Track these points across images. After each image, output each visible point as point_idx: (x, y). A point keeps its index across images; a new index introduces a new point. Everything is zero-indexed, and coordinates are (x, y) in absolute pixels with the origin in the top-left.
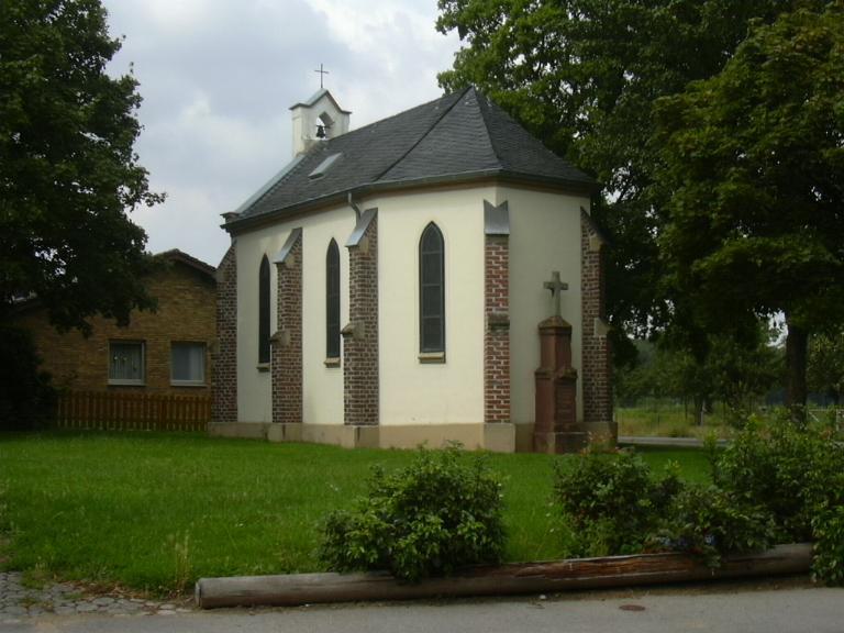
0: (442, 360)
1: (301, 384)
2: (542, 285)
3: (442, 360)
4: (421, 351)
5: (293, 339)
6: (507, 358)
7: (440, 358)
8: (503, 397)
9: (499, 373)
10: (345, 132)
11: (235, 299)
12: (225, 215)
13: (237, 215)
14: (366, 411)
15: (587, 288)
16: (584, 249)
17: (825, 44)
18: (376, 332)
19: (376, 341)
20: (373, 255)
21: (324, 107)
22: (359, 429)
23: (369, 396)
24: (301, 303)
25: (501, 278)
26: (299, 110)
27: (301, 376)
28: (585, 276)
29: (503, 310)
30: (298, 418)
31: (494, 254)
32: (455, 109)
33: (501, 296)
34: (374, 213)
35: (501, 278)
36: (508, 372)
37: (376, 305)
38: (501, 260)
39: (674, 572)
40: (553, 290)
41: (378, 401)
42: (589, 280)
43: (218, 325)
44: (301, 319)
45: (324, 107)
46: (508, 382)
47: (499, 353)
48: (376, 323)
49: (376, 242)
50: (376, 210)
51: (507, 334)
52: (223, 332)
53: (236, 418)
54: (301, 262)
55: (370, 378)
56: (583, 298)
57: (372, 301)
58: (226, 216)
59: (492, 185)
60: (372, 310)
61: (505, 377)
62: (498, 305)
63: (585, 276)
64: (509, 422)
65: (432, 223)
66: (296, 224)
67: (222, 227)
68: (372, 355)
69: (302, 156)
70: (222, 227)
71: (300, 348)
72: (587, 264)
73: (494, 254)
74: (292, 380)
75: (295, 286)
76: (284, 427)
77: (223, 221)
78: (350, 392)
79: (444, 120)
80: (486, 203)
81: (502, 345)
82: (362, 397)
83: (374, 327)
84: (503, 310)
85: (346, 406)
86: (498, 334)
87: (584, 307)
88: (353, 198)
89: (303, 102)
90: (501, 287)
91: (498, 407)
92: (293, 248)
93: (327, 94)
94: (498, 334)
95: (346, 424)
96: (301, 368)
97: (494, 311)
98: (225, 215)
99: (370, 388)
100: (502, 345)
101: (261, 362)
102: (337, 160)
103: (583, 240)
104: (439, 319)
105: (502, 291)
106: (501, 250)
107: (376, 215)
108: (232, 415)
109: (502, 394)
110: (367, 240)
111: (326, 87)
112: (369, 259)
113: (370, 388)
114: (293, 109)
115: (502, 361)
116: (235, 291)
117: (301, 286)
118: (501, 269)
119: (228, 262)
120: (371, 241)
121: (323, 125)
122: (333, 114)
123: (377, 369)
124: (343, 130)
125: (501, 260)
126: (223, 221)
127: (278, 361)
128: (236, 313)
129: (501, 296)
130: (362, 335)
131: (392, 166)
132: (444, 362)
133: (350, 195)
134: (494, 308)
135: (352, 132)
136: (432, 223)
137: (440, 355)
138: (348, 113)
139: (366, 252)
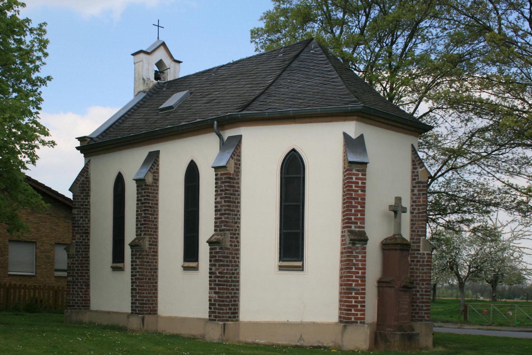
0: (301, 269)
1: (156, 283)
2: (388, 208)
3: (301, 269)
4: (281, 259)
5: (150, 245)
6: (365, 269)
7: (299, 267)
8: (359, 302)
9: (357, 281)
10: (177, 78)
11: (89, 209)
12: (80, 139)
13: (91, 139)
14: (230, 309)
15: (416, 211)
16: (413, 179)
17: (530, 39)
18: (238, 242)
19: (238, 250)
20: (238, 176)
21: (160, 54)
22: (224, 324)
23: (232, 297)
24: (157, 215)
25: (360, 200)
26: (142, 55)
27: (157, 276)
28: (414, 202)
29: (359, 227)
30: (154, 311)
31: (354, 180)
32: (303, 56)
33: (359, 216)
34: (238, 140)
35: (360, 200)
36: (365, 281)
37: (239, 219)
38: (360, 184)
39: (12, 297)
40: (396, 212)
41: (238, 301)
42: (416, 205)
43: (74, 230)
44: (157, 228)
45: (160, 54)
46: (364, 289)
47: (358, 265)
48: (239, 234)
49: (240, 165)
50: (241, 136)
51: (365, 248)
52: (78, 236)
53: (89, 306)
54: (158, 180)
55: (233, 281)
56: (412, 220)
57: (236, 215)
58: (81, 139)
59: (353, 120)
60: (236, 223)
61: (361, 285)
62: (356, 223)
63: (414, 202)
64: (364, 323)
65: (294, 150)
66: (153, 148)
67: (78, 148)
68: (235, 262)
69: (143, 95)
70: (78, 148)
71: (156, 253)
72: (416, 192)
73: (360, 182)
74: (149, 279)
75: (153, 200)
76: (143, 319)
77: (78, 144)
78: (215, 293)
79: (294, 65)
80: (345, 134)
81: (360, 258)
82: (228, 297)
83: (237, 238)
84: (359, 227)
85: (210, 304)
86: (357, 248)
87: (412, 228)
88: (218, 126)
89: (144, 49)
90: (359, 208)
91: (355, 311)
92: (151, 168)
93: (163, 44)
94: (357, 248)
95: (210, 320)
96: (157, 269)
97: (353, 228)
98: (80, 139)
99: (233, 289)
100: (360, 258)
101: (114, 262)
102: (185, 96)
103: (413, 172)
104: (298, 233)
105: (359, 211)
106: (360, 176)
107: (240, 142)
108: (86, 303)
109: (360, 299)
110: (232, 162)
111: (162, 39)
112: (234, 179)
113: (233, 289)
114: (134, 54)
115: (360, 271)
116: (89, 202)
117: (157, 200)
118: (360, 192)
119: (83, 178)
120: (236, 164)
121: (158, 70)
122: (167, 62)
123: (238, 274)
124: (174, 76)
125: (360, 184)
126: (78, 144)
127: (138, 263)
128: (89, 221)
129: (359, 216)
130: (228, 244)
131: (254, 100)
132: (303, 270)
133: (216, 123)
134: (353, 226)
135: (170, 81)
136: (294, 150)
137: (299, 264)
138: (179, 62)
139: (232, 172)
